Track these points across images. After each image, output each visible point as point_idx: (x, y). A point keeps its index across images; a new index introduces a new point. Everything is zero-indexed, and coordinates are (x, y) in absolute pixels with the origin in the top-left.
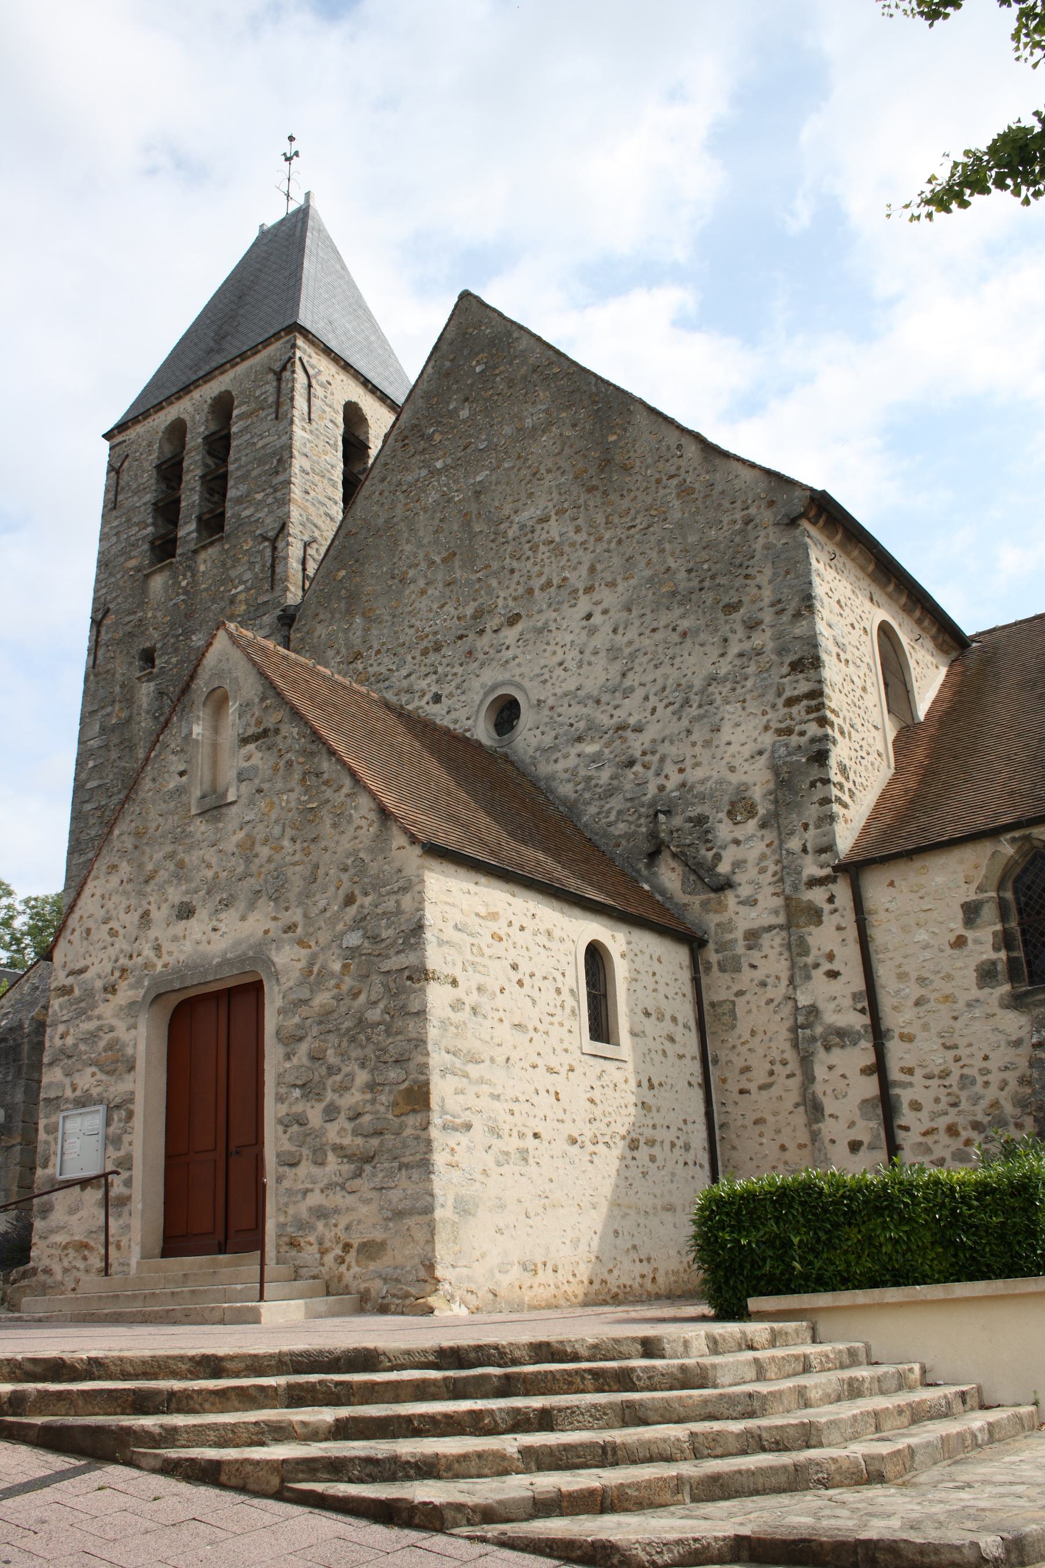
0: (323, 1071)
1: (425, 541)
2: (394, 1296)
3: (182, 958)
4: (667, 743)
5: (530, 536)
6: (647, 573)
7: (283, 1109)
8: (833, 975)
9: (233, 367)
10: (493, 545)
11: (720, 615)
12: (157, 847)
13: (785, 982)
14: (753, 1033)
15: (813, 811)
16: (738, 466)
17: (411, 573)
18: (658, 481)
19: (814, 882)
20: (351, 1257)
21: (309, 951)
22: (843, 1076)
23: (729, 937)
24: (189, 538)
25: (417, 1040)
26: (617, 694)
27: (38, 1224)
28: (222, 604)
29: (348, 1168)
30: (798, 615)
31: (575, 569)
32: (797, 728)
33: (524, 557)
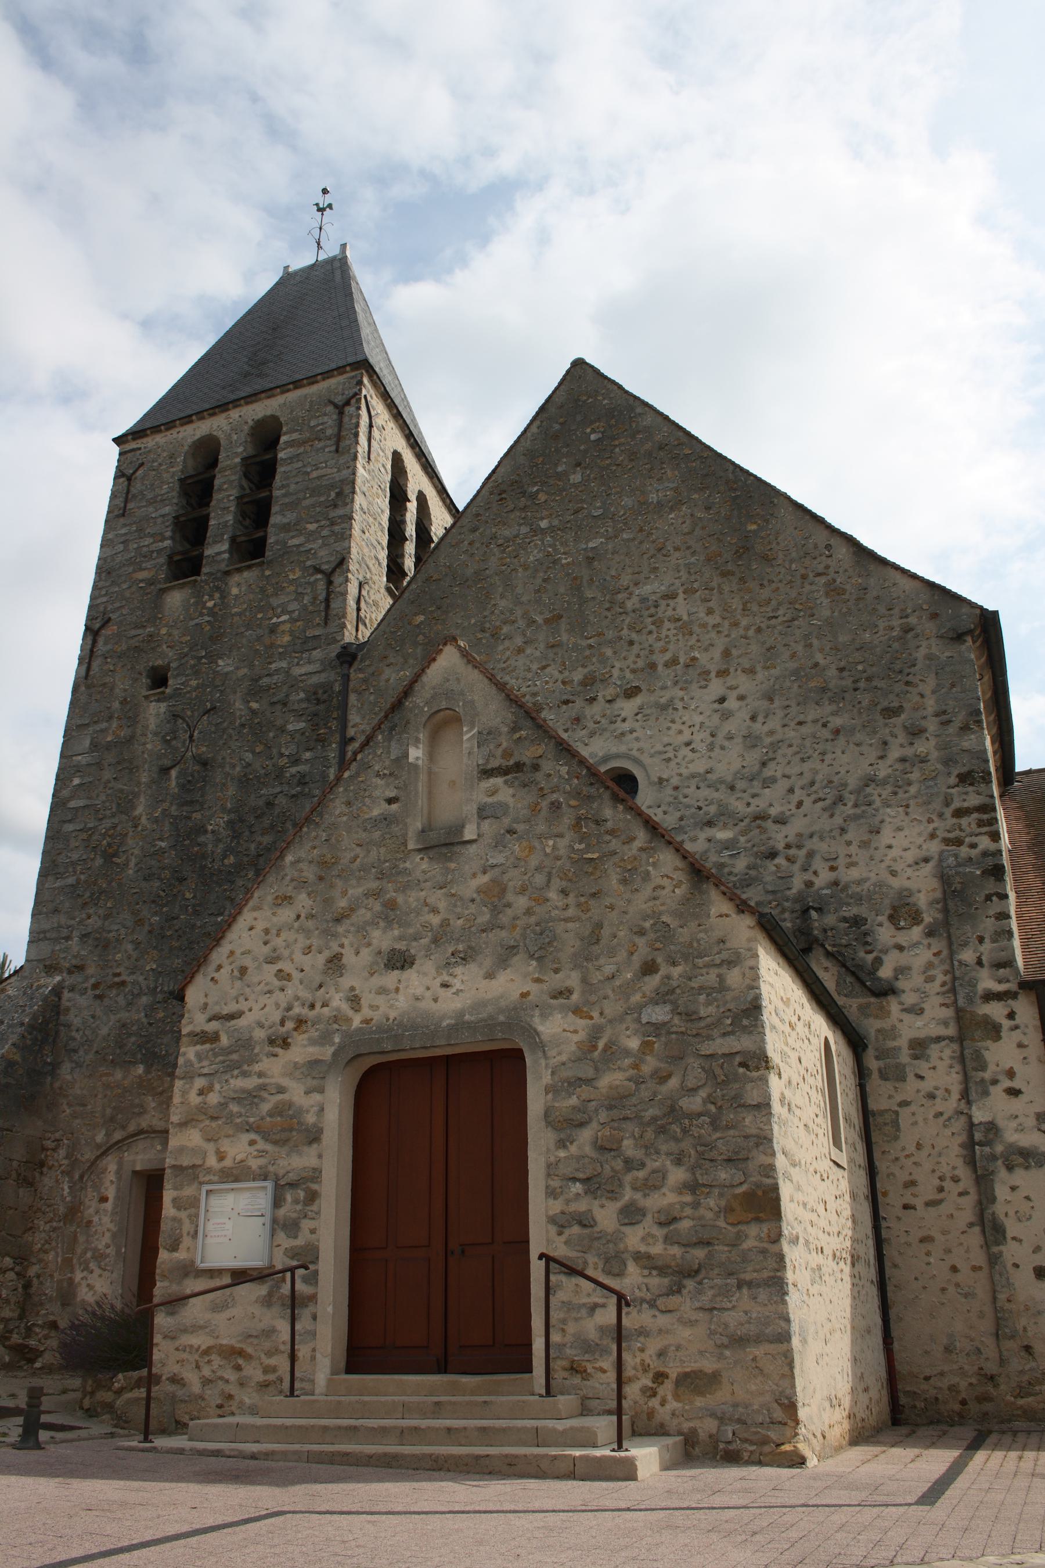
0: (619, 1165)
1: (524, 599)
2: (745, 1440)
3: (392, 1015)
4: (815, 839)
5: (652, 610)
6: (792, 665)
7: (556, 1206)
8: (1014, 1092)
9: (283, 393)
10: (609, 614)
11: (878, 717)
12: (354, 882)
13: (955, 1096)
14: (919, 1146)
15: (988, 925)
16: (898, 575)
17: (505, 629)
18: (804, 577)
19: (990, 996)
20: (666, 1389)
21: (588, 1021)
22: (1028, 1198)
23: (891, 1044)
24: (218, 558)
25: (758, 1136)
26: (755, 783)
27: (161, 1320)
28: (260, 632)
29: (656, 1282)
30: (965, 728)
31: (706, 650)
32: (967, 840)
33: (645, 631)
